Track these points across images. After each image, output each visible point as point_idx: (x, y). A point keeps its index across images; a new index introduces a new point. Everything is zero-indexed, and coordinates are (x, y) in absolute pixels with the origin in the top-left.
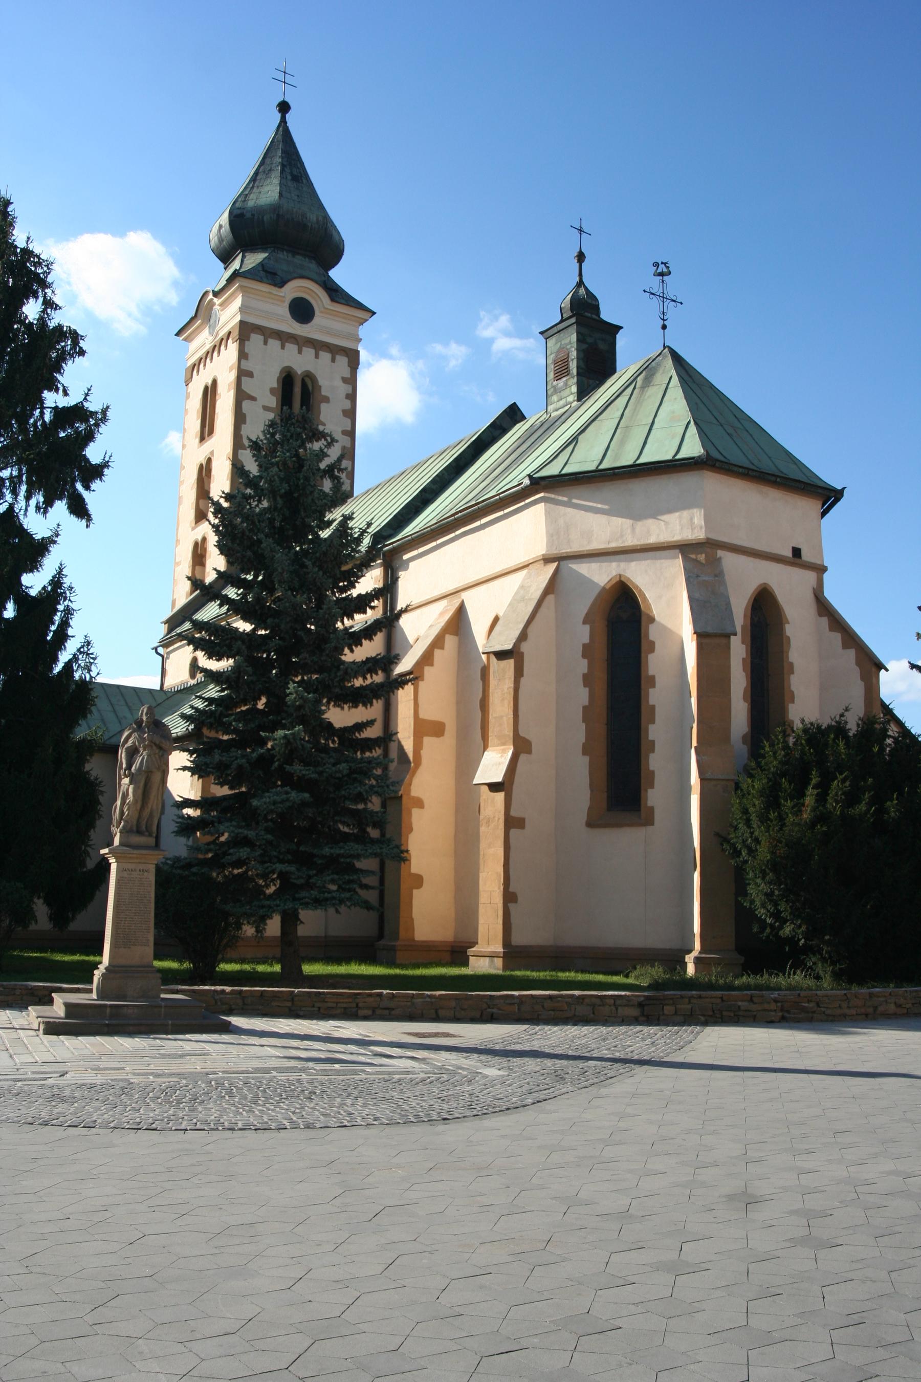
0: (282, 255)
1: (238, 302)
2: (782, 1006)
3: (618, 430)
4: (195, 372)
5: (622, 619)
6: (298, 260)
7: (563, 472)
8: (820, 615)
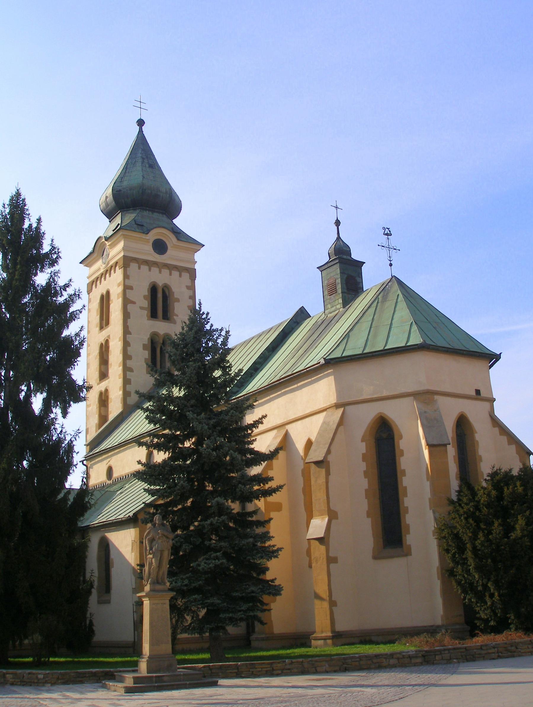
0: (146, 213)
1: (121, 245)
2: (498, 650)
3: (372, 329)
4: (94, 286)
5: (384, 437)
6: (156, 215)
7: (343, 355)
8: (494, 426)
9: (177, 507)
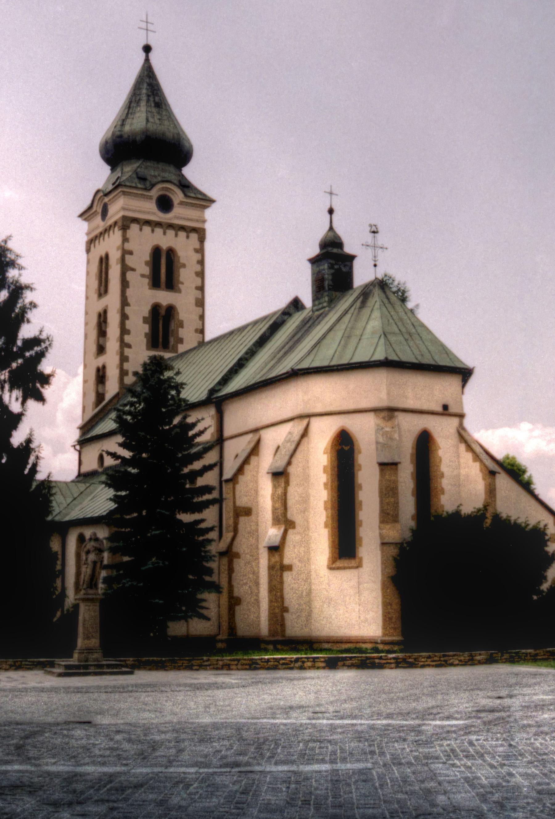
8: (461, 442)
9: (170, 498)
